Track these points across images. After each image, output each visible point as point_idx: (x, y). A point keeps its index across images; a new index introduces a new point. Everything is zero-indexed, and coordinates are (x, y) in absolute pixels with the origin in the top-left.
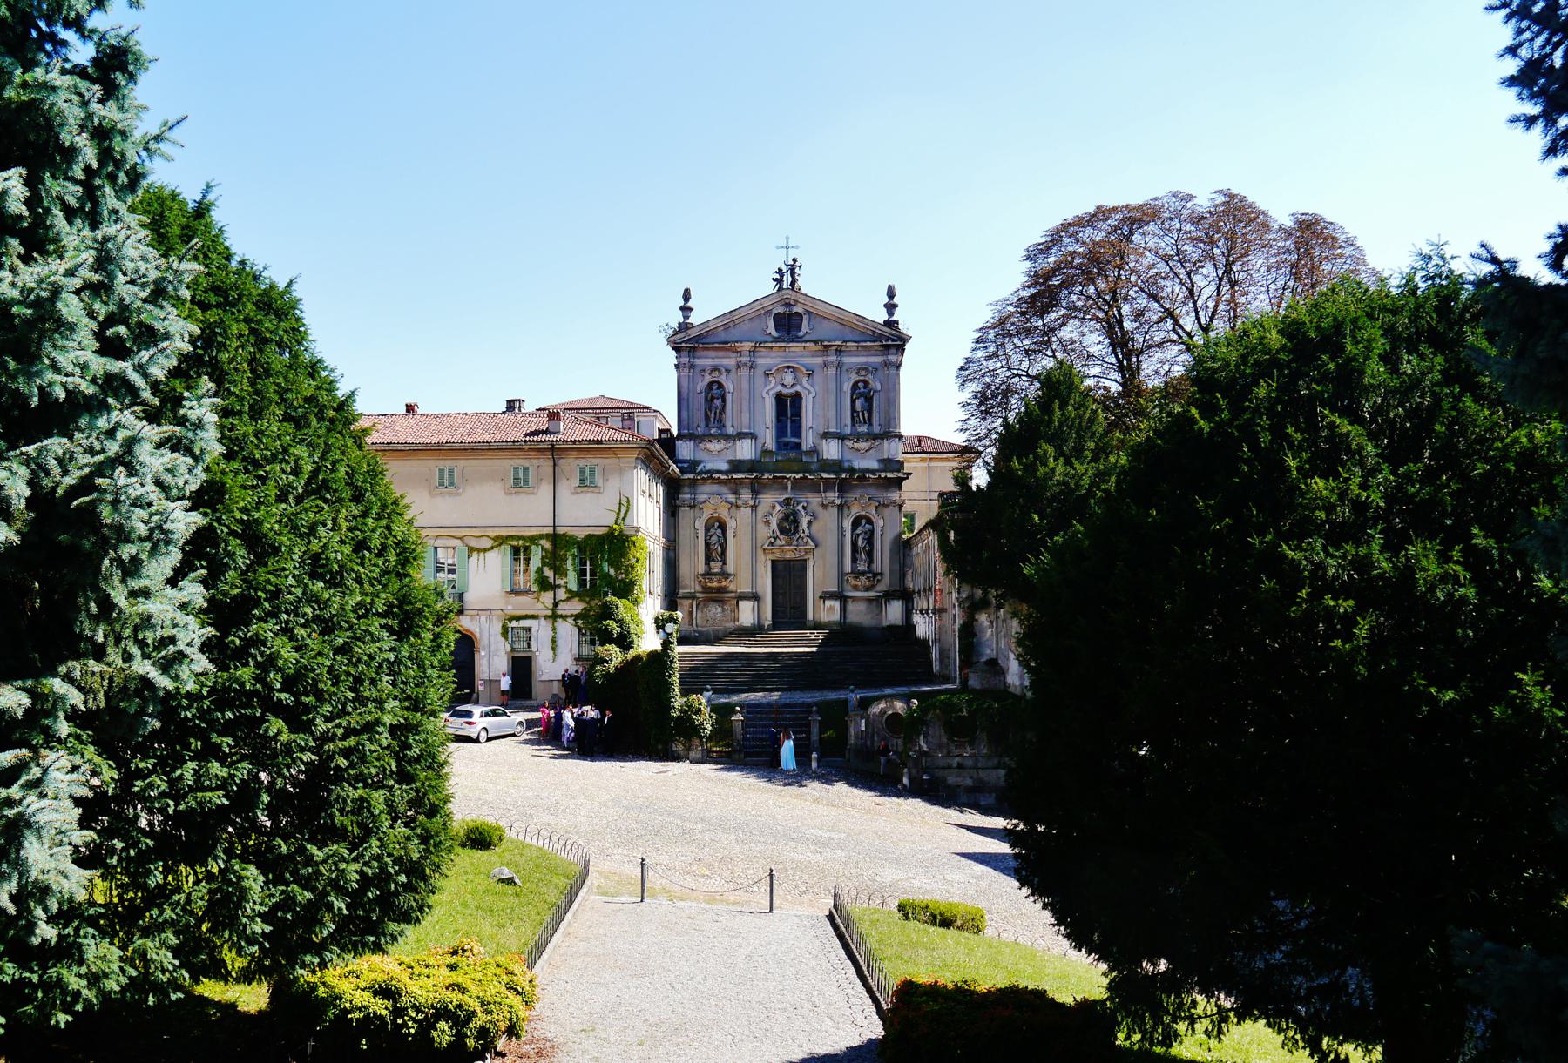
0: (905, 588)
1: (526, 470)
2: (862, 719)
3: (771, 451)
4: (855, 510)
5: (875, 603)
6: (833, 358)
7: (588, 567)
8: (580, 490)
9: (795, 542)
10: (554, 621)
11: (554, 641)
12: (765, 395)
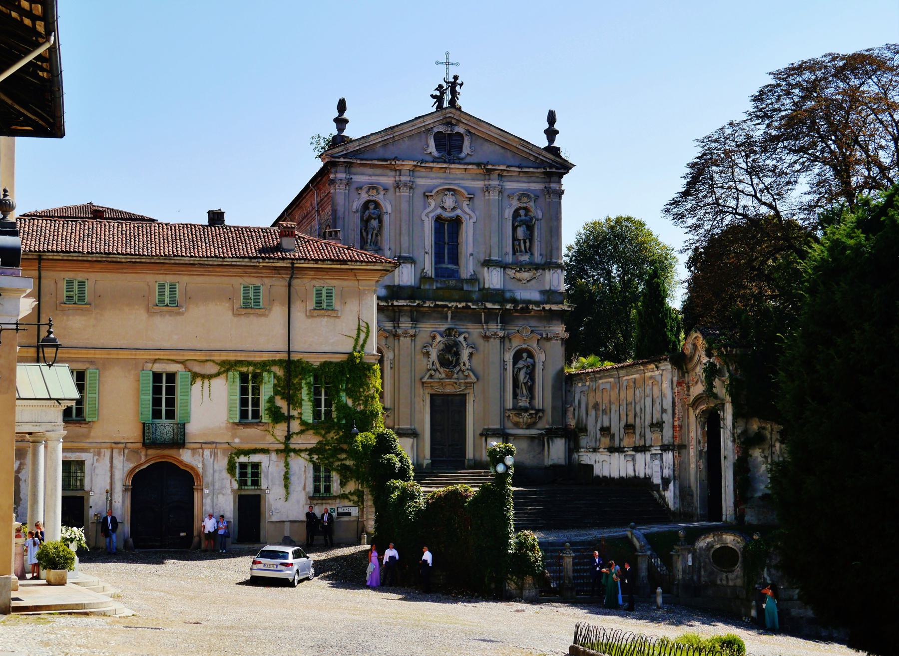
0: (566, 426)
1: (257, 289)
2: (689, 553)
3: (431, 278)
4: (516, 344)
5: (537, 441)
6: (495, 183)
7: (323, 397)
8: (316, 313)
9: (455, 376)
10: (287, 456)
11: (286, 477)
12: (424, 217)
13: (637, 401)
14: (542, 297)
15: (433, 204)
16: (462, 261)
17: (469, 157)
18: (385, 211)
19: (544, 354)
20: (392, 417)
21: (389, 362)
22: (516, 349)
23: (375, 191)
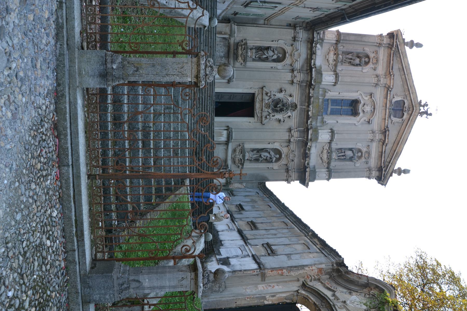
4: (284, 151)
13: (277, 230)
14: (312, 167)
15: (366, 98)
16: (334, 117)
17: (391, 121)
18: (364, 68)
19: (278, 168)
22: (280, 149)
23: (375, 62)
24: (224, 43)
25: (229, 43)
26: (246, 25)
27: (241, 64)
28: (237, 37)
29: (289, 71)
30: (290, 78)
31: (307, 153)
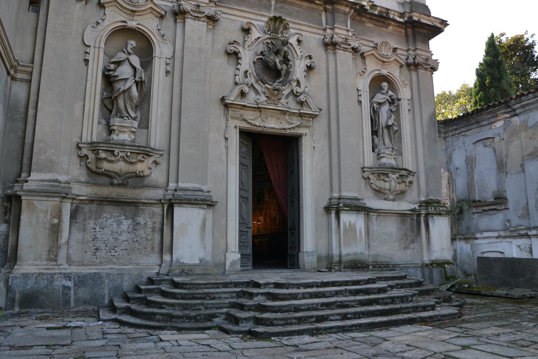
5: (409, 220)
20: (163, 166)
21: (163, 62)
24: (90, 218)
25: (91, 201)
26: (28, 140)
27: (156, 163)
28: (68, 173)
29: (179, 26)
30: (202, 26)
31: (380, 11)
